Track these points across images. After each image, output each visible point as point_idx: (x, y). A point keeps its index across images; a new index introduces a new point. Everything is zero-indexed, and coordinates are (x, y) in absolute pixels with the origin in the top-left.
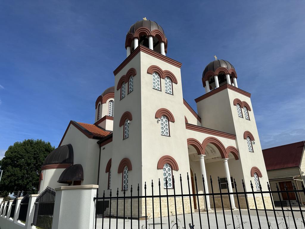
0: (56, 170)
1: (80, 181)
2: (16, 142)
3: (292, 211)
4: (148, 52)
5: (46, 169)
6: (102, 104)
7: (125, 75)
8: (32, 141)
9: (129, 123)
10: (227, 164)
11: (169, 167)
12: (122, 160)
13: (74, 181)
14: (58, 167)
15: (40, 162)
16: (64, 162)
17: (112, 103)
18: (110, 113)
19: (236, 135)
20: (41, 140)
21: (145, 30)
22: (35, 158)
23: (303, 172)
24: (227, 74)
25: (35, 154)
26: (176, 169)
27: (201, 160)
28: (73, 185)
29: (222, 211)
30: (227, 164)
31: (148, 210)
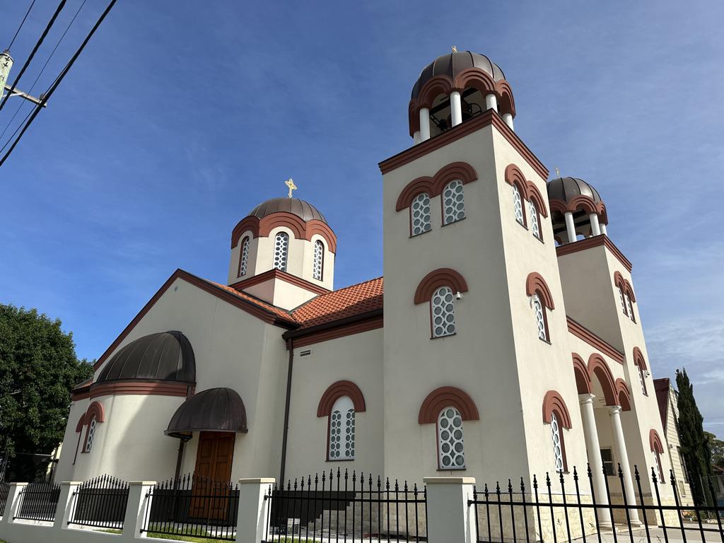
0: (145, 404)
1: (234, 435)
2: (27, 310)
3: (702, 530)
4: (509, 138)
5: (115, 395)
6: (256, 236)
7: (432, 176)
8: (11, 309)
9: (458, 299)
10: (618, 417)
11: (443, 415)
12: (336, 383)
13: (201, 432)
14: (152, 393)
15: (33, 369)
16: (172, 377)
17: (282, 239)
18: (277, 264)
19: (624, 355)
20: (35, 311)
21: (482, 76)
22: (19, 359)
23: (671, 445)
24: (594, 212)
25: (18, 348)
26: (568, 426)
27: (585, 406)
28: (601, 450)
29: (628, 530)
30: (618, 417)
31: (577, 524)
